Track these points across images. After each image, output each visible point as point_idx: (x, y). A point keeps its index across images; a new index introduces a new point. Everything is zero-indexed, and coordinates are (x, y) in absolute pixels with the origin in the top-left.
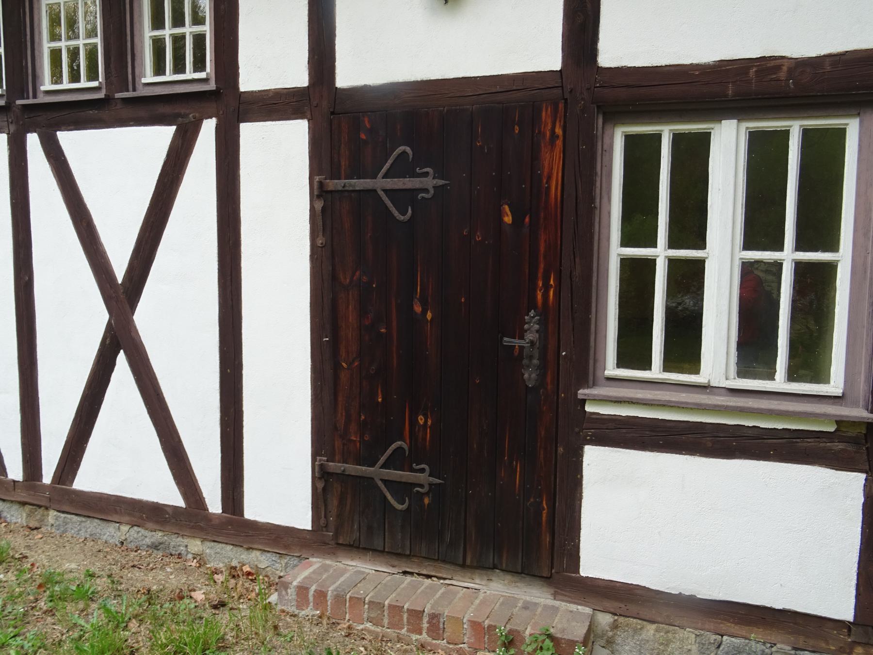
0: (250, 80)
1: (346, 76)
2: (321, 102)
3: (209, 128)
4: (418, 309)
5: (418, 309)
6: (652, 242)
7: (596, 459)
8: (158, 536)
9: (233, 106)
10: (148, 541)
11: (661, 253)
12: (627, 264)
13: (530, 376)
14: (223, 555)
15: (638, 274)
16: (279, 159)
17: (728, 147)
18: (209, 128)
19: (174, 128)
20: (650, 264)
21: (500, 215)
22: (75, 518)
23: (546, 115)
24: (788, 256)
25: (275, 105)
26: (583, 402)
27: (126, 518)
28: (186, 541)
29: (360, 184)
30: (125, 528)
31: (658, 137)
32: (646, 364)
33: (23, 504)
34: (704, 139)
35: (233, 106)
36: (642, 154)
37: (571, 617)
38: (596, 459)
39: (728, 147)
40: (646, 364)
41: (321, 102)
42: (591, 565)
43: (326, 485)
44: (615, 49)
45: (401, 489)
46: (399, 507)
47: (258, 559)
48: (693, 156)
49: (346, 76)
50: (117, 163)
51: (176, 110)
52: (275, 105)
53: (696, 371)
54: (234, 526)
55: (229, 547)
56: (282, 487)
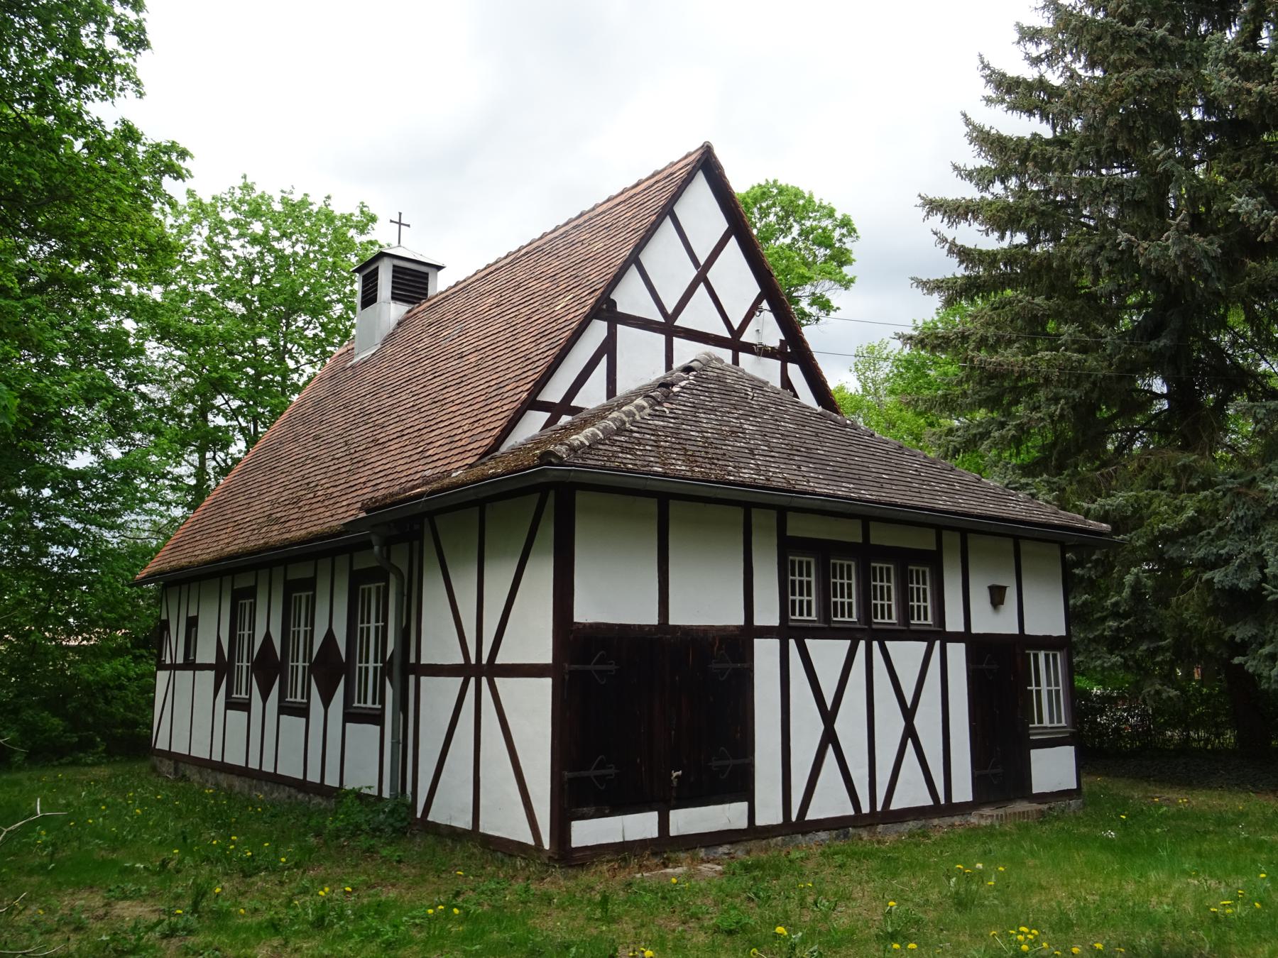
0: (949, 629)
2: (966, 636)
7: (1034, 753)
16: (957, 652)
18: (938, 643)
25: (955, 637)
37: (1035, 806)
38: (1034, 753)
42: (1036, 790)
44: (1029, 631)
50: (907, 654)
52: (955, 637)
56: (963, 791)
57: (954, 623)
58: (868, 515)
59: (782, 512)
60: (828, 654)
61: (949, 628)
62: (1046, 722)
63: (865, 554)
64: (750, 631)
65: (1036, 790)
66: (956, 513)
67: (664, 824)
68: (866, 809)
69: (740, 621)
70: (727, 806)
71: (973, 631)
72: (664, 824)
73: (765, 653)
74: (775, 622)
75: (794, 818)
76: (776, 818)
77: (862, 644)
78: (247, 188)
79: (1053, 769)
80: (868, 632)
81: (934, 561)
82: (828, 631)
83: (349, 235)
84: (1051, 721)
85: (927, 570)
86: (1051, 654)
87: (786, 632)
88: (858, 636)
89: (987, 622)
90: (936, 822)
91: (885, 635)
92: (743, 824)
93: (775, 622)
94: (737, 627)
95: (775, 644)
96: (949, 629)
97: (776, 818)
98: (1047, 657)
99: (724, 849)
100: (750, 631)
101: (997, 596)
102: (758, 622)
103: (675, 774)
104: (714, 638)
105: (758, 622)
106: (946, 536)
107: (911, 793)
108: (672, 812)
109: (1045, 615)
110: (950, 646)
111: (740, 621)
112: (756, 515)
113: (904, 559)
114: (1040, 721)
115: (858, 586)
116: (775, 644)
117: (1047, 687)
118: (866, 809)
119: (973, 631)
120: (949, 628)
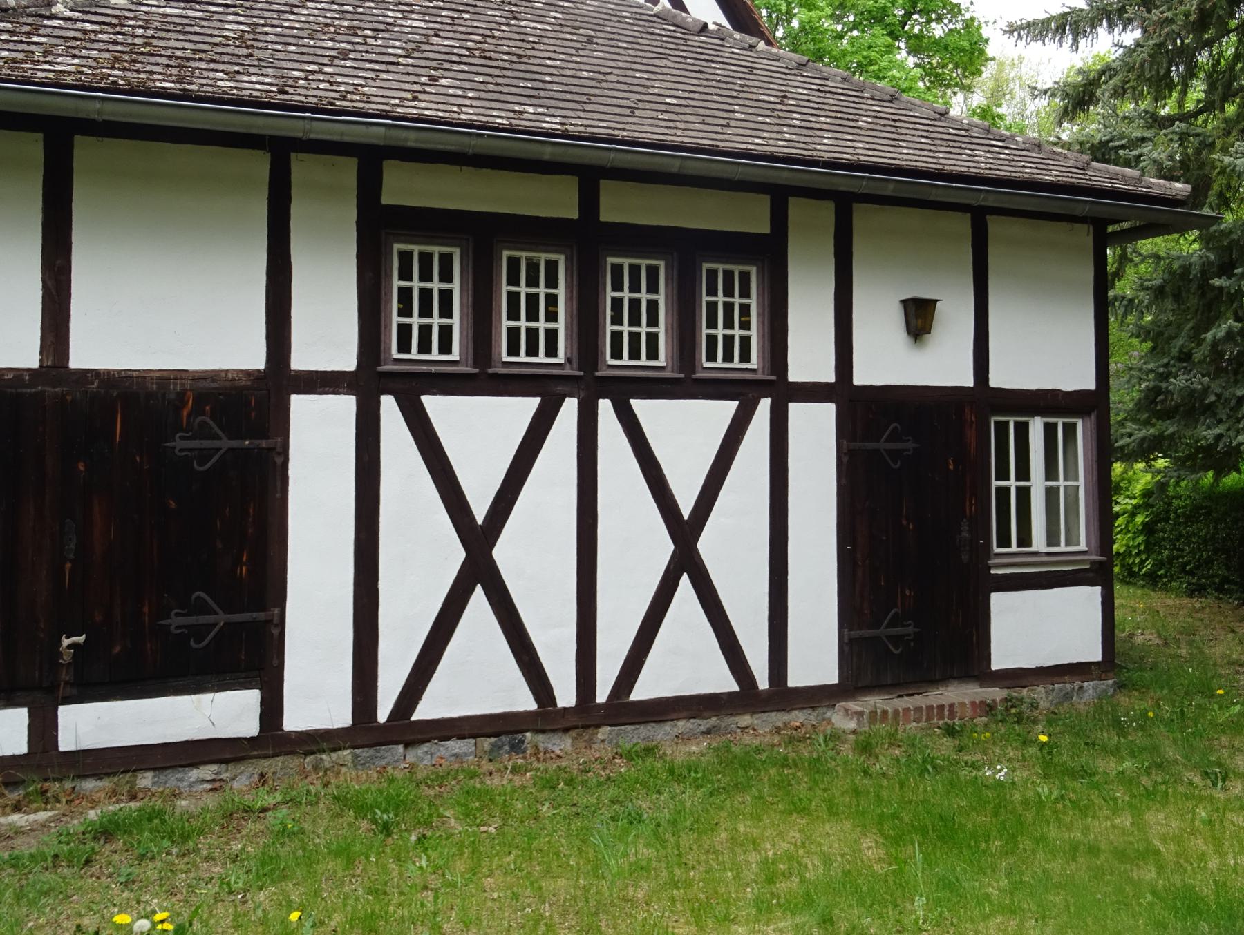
0: (794, 375)
1: (860, 378)
2: (841, 391)
3: (765, 405)
4: (904, 522)
5: (904, 522)
6: (1008, 479)
7: (999, 601)
8: (713, 721)
9: (785, 393)
10: (703, 728)
11: (1013, 483)
12: (510, 330)
13: (965, 557)
14: (634, 736)
15: (1003, 493)
16: (815, 430)
17: (1036, 427)
18: (765, 405)
19: (737, 403)
20: (1008, 489)
21: (948, 465)
22: (629, 728)
23: (967, 411)
24: (1061, 483)
25: (812, 392)
26: (990, 568)
27: (684, 714)
28: (737, 719)
29: (870, 445)
30: (681, 723)
31: (1007, 423)
32: (1009, 545)
33: (566, 730)
34: (1026, 425)
35: (785, 393)
36: (1002, 428)
37: (995, 694)
38: (999, 601)
39: (1036, 427)
40: (1009, 545)
41: (841, 391)
42: (999, 662)
43: (849, 650)
44: (999, 379)
45: (896, 640)
46: (896, 652)
47: (797, 717)
48: (1022, 431)
49: (860, 378)
50: (685, 431)
51: (743, 392)
52: (812, 392)
53: (1030, 545)
54: (782, 695)
55: (773, 714)
56: (815, 657)
57: (810, 358)
58: (592, 170)
59: (371, 160)
60: (481, 431)
61: (797, 373)
62: (1039, 541)
63: (588, 243)
64: (278, 382)
65: (999, 662)
66: (815, 163)
67: (43, 730)
68: (566, 696)
69: (254, 358)
70: (207, 697)
71: (858, 380)
72: (43, 730)
73: (319, 434)
74: (347, 361)
75: (383, 715)
76: (336, 712)
77: (570, 409)
78: (987, 41)
79: (1040, 628)
80: (591, 382)
81: (769, 256)
82: (482, 380)
83: (1195, 82)
84: (1052, 538)
85: (753, 271)
86: (1060, 422)
87: (367, 382)
88: (560, 389)
89: (885, 360)
90: (745, 720)
91: (625, 390)
92: (249, 726)
93: (347, 361)
94: (248, 373)
95: (345, 406)
96: (794, 375)
97: (336, 712)
98: (1050, 431)
99: (207, 772)
100: (278, 382)
101: (919, 318)
102: (300, 361)
103: (66, 642)
104: (182, 395)
105: (300, 361)
106: (797, 209)
107: (686, 662)
108: (63, 711)
109: (1045, 344)
110: (797, 411)
111: (254, 358)
112: (302, 168)
113: (686, 251)
114: (1025, 540)
115: (569, 299)
116: (345, 406)
117: (1048, 492)
118: (566, 696)
119: (858, 380)
120: (797, 373)
